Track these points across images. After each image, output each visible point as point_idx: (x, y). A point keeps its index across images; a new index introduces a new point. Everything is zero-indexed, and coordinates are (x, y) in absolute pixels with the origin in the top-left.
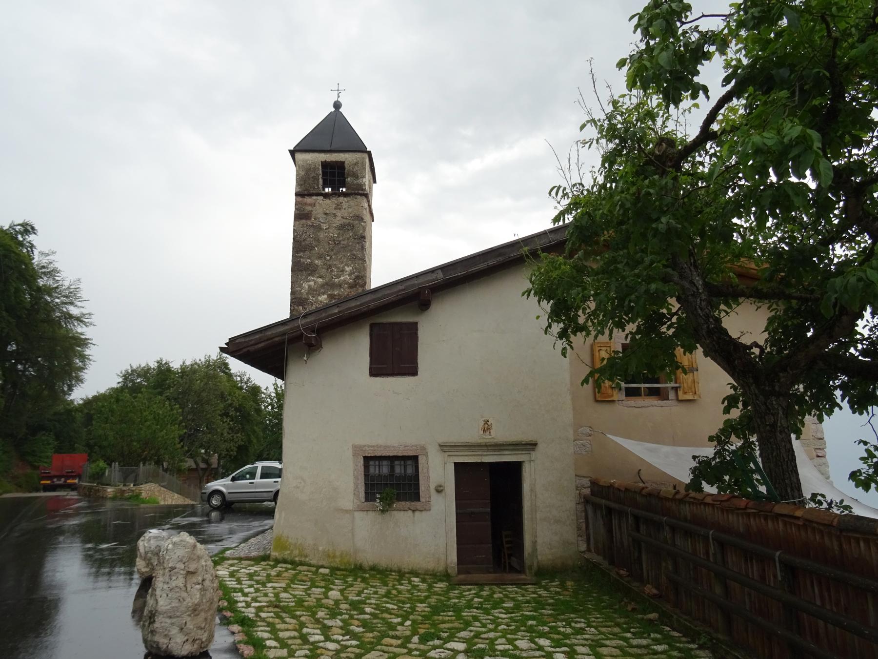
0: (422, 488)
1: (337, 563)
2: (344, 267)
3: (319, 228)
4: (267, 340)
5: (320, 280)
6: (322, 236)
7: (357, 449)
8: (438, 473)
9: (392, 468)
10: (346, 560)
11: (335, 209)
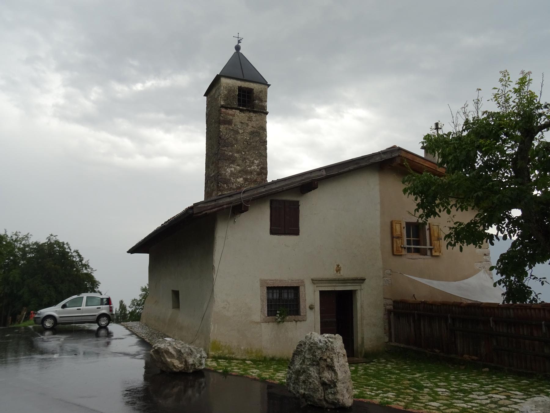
1: (254, 356)
2: (253, 160)
3: (237, 132)
5: (238, 168)
6: (239, 138)
7: (263, 282)
8: (310, 297)
11: (248, 120)
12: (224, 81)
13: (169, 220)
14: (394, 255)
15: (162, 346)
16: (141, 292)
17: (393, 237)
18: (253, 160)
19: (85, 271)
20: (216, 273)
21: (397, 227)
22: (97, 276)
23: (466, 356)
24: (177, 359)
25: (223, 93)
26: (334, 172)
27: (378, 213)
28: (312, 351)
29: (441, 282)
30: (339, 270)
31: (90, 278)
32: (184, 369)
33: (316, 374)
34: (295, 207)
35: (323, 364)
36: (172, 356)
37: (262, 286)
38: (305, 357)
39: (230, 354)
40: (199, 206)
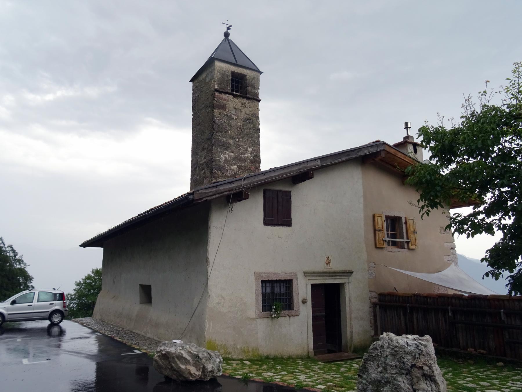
0: (295, 301)
2: (247, 148)
4: (221, 193)
5: (232, 154)
6: (233, 123)
8: (303, 291)
9: (273, 288)
10: (256, 354)
12: (217, 64)
13: (151, 209)
14: (376, 247)
15: (172, 350)
16: (75, 287)
17: (375, 231)
18: (247, 148)
19: (18, 266)
20: (211, 265)
21: (379, 220)
22: (30, 271)
23: (471, 350)
24: (193, 366)
25: (217, 76)
26: (328, 162)
27: (362, 206)
28: (398, 356)
29: (423, 274)
30: (329, 263)
31: (23, 273)
32: (200, 378)
33: (408, 386)
34: (288, 196)
35: (416, 373)
36: (186, 362)
37: (256, 280)
38: (387, 365)
39: (226, 353)
40: (200, 192)
